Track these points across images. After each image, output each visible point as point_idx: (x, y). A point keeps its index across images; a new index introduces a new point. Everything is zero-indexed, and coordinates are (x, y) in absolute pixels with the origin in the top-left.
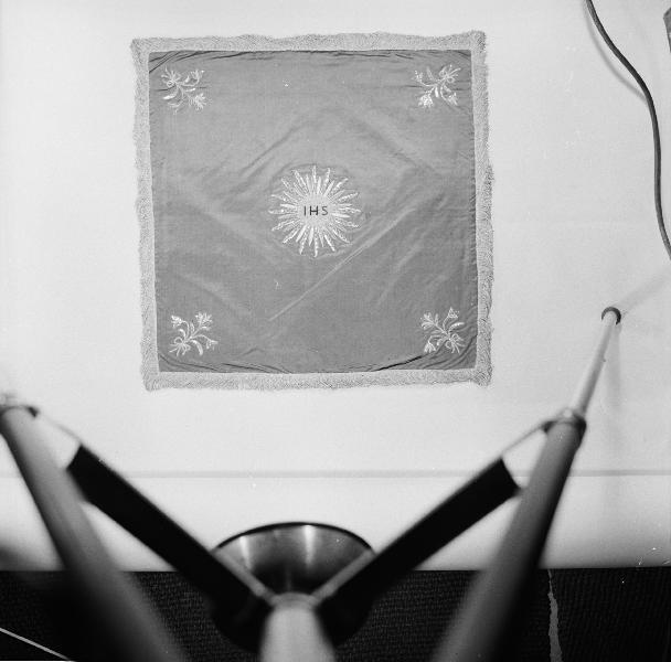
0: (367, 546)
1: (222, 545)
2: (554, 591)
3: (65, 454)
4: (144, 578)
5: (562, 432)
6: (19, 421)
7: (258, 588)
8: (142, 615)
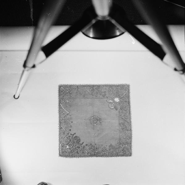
0: (84, 33)
1: (123, 33)
2: (32, 21)
3: (168, 58)
4: (144, 23)
5: (30, 64)
6: (179, 67)
7: (113, 22)
8: (145, 15)
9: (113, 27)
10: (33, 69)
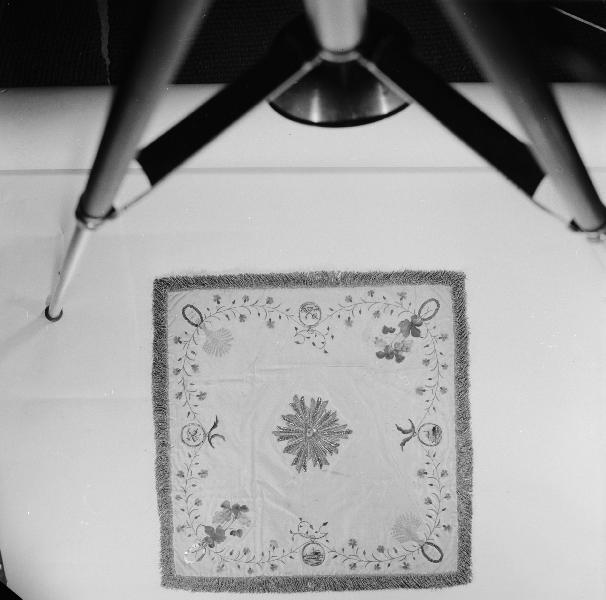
0: (273, 106)
1: (404, 106)
4: (476, 77)
5: (99, 208)
6: (587, 219)
7: (372, 68)
9: (370, 82)
10: (109, 224)
